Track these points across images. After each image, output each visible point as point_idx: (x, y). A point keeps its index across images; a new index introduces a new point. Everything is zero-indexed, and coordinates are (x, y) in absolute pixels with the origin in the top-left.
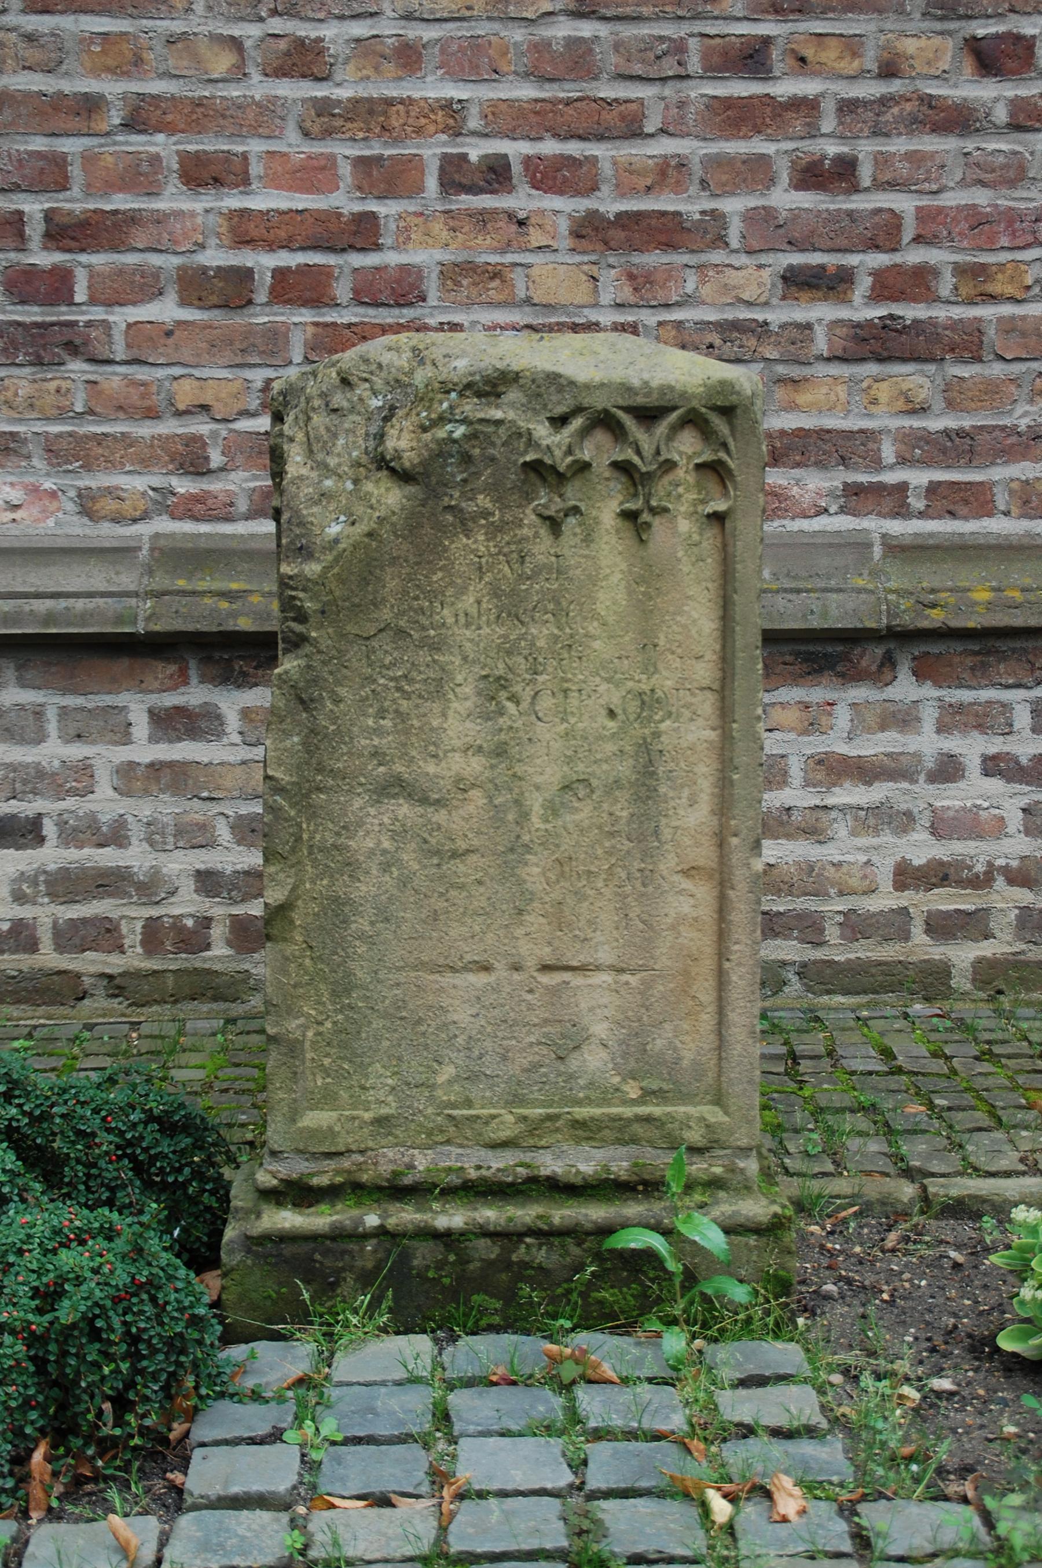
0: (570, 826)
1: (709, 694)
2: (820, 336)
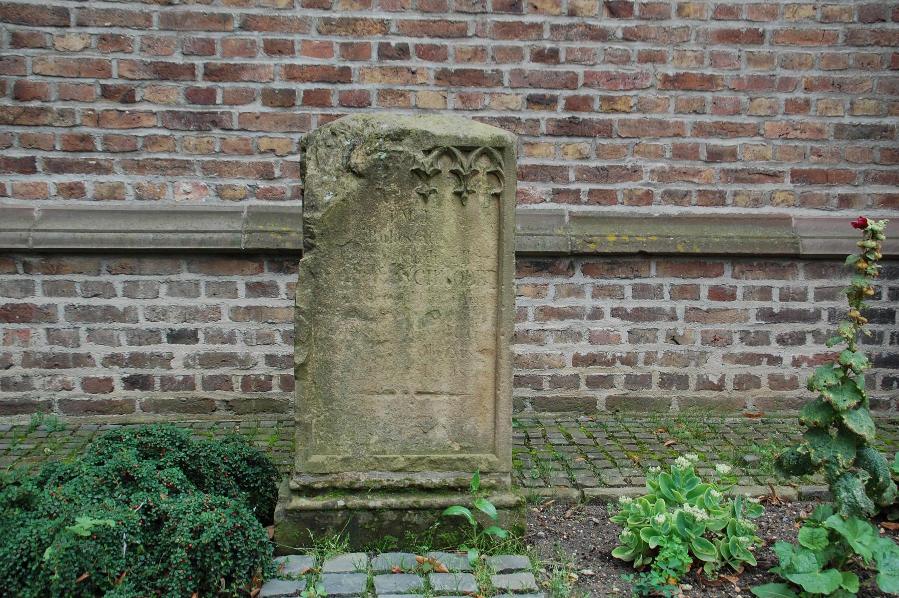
0: (430, 331)
1: (492, 273)
2: (543, 125)
